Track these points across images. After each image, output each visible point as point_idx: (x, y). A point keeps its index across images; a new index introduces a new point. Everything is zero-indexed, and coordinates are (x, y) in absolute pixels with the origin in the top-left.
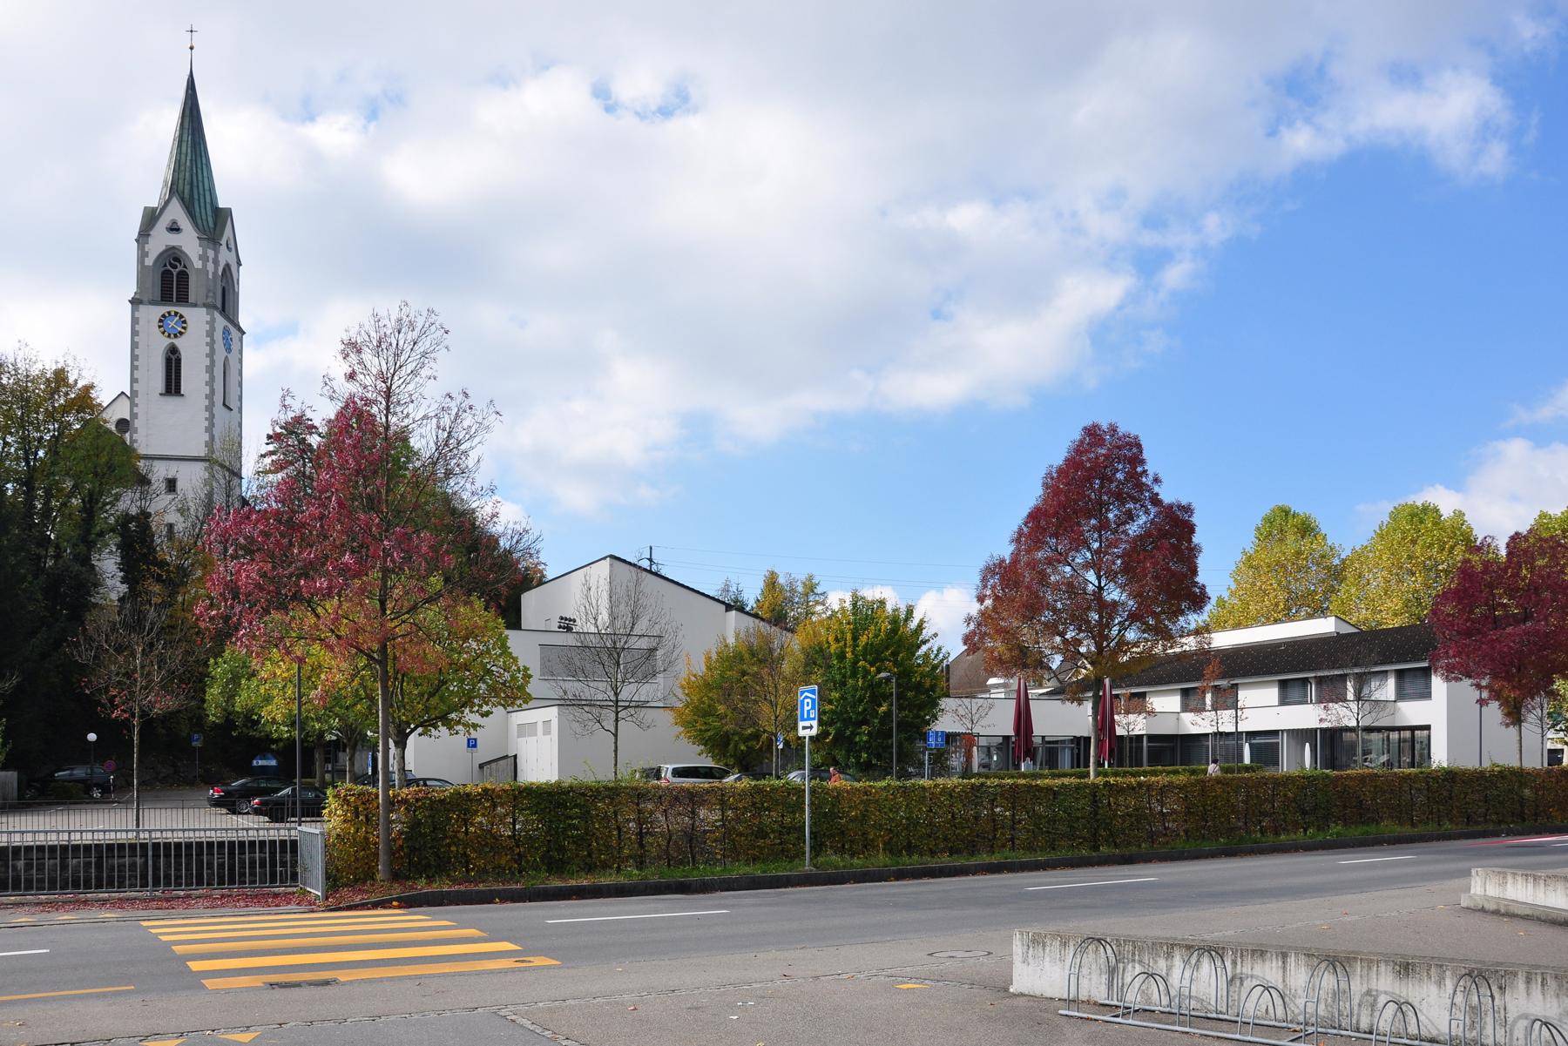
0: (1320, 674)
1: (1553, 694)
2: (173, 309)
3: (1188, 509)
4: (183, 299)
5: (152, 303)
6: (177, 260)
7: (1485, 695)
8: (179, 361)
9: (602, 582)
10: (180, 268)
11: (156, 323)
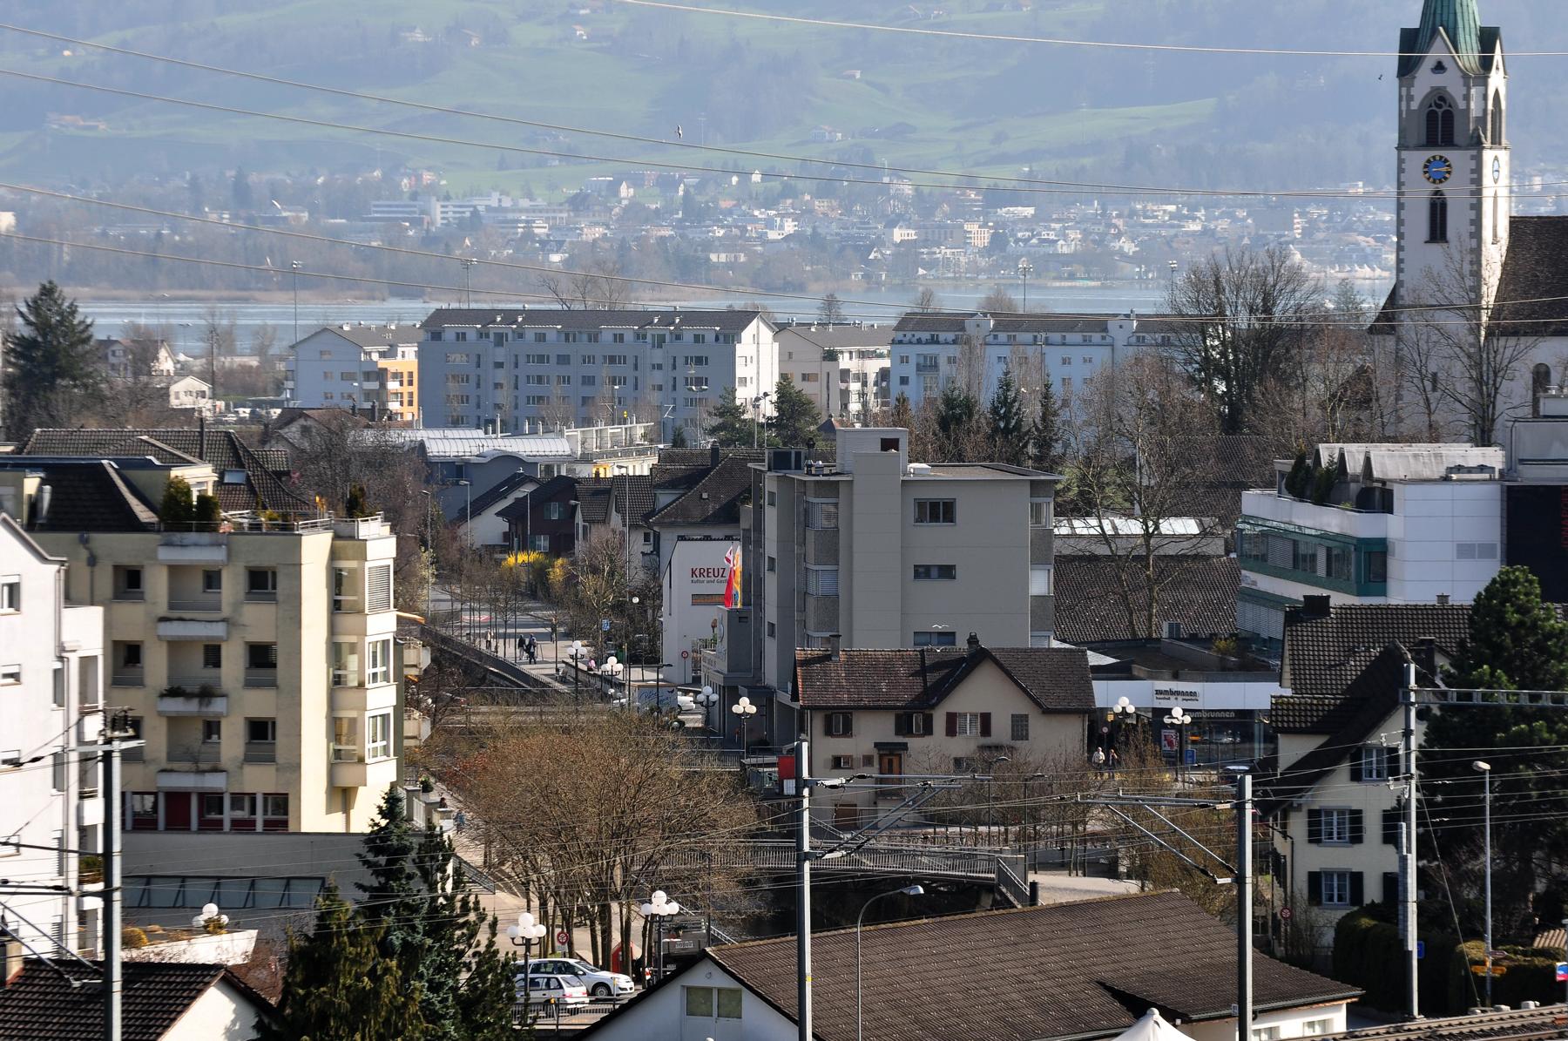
0: (863, 348)
1: (1564, 926)
2: (1437, 153)
3: (1403, 30)
4: (1449, 142)
5: (1419, 147)
6: (1442, 99)
7: (820, 445)
8: (1444, 205)
9: (1033, 296)
10: (1445, 108)
11: (1420, 169)
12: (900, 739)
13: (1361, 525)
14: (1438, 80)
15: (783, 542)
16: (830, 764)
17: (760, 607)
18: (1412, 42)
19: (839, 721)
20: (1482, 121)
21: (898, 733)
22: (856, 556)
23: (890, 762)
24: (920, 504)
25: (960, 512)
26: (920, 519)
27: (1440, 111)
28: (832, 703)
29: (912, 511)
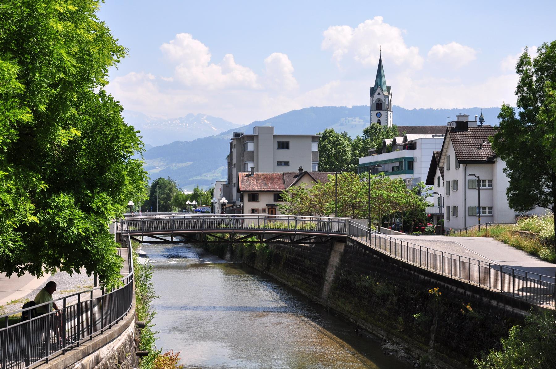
4: (381, 109)
12: (275, 203)
13: (407, 153)
14: (379, 97)
15: (238, 158)
16: (251, 211)
17: (232, 179)
18: (373, 91)
19: (254, 197)
20: (388, 105)
21: (275, 201)
22: (259, 158)
23: (272, 211)
24: (279, 144)
25: (291, 145)
26: (279, 147)
28: (251, 190)
29: (276, 145)
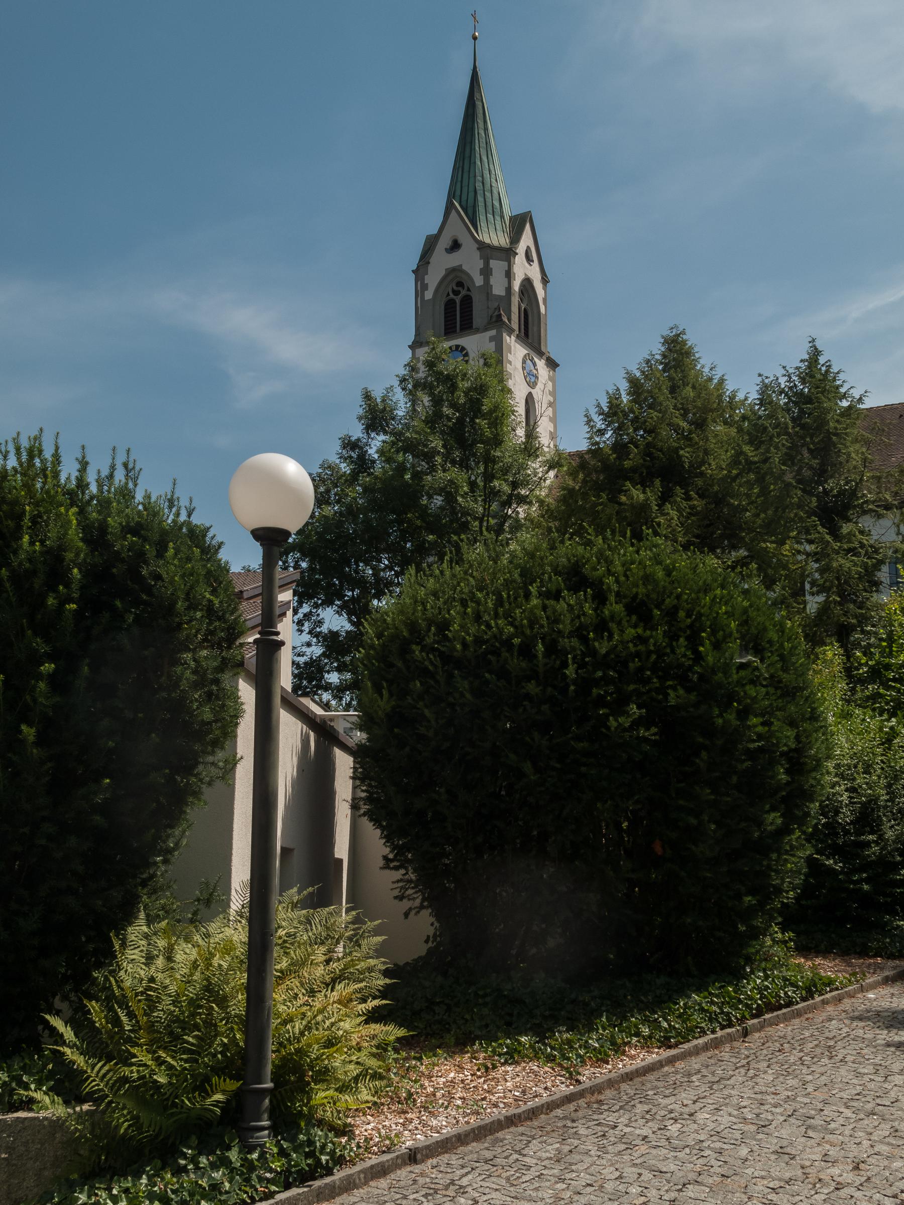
6: (460, 284)
10: (463, 292)
14: (454, 260)
27: (458, 300)
